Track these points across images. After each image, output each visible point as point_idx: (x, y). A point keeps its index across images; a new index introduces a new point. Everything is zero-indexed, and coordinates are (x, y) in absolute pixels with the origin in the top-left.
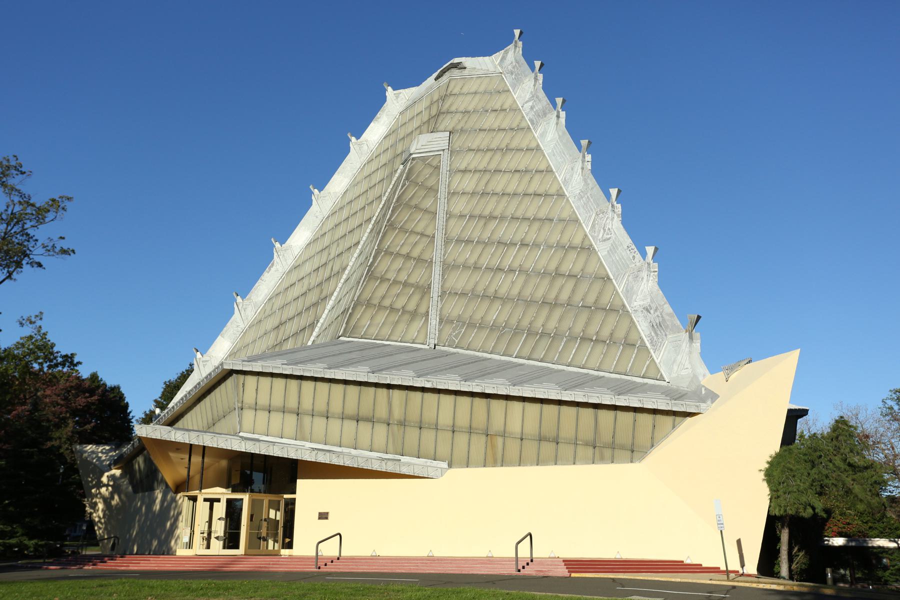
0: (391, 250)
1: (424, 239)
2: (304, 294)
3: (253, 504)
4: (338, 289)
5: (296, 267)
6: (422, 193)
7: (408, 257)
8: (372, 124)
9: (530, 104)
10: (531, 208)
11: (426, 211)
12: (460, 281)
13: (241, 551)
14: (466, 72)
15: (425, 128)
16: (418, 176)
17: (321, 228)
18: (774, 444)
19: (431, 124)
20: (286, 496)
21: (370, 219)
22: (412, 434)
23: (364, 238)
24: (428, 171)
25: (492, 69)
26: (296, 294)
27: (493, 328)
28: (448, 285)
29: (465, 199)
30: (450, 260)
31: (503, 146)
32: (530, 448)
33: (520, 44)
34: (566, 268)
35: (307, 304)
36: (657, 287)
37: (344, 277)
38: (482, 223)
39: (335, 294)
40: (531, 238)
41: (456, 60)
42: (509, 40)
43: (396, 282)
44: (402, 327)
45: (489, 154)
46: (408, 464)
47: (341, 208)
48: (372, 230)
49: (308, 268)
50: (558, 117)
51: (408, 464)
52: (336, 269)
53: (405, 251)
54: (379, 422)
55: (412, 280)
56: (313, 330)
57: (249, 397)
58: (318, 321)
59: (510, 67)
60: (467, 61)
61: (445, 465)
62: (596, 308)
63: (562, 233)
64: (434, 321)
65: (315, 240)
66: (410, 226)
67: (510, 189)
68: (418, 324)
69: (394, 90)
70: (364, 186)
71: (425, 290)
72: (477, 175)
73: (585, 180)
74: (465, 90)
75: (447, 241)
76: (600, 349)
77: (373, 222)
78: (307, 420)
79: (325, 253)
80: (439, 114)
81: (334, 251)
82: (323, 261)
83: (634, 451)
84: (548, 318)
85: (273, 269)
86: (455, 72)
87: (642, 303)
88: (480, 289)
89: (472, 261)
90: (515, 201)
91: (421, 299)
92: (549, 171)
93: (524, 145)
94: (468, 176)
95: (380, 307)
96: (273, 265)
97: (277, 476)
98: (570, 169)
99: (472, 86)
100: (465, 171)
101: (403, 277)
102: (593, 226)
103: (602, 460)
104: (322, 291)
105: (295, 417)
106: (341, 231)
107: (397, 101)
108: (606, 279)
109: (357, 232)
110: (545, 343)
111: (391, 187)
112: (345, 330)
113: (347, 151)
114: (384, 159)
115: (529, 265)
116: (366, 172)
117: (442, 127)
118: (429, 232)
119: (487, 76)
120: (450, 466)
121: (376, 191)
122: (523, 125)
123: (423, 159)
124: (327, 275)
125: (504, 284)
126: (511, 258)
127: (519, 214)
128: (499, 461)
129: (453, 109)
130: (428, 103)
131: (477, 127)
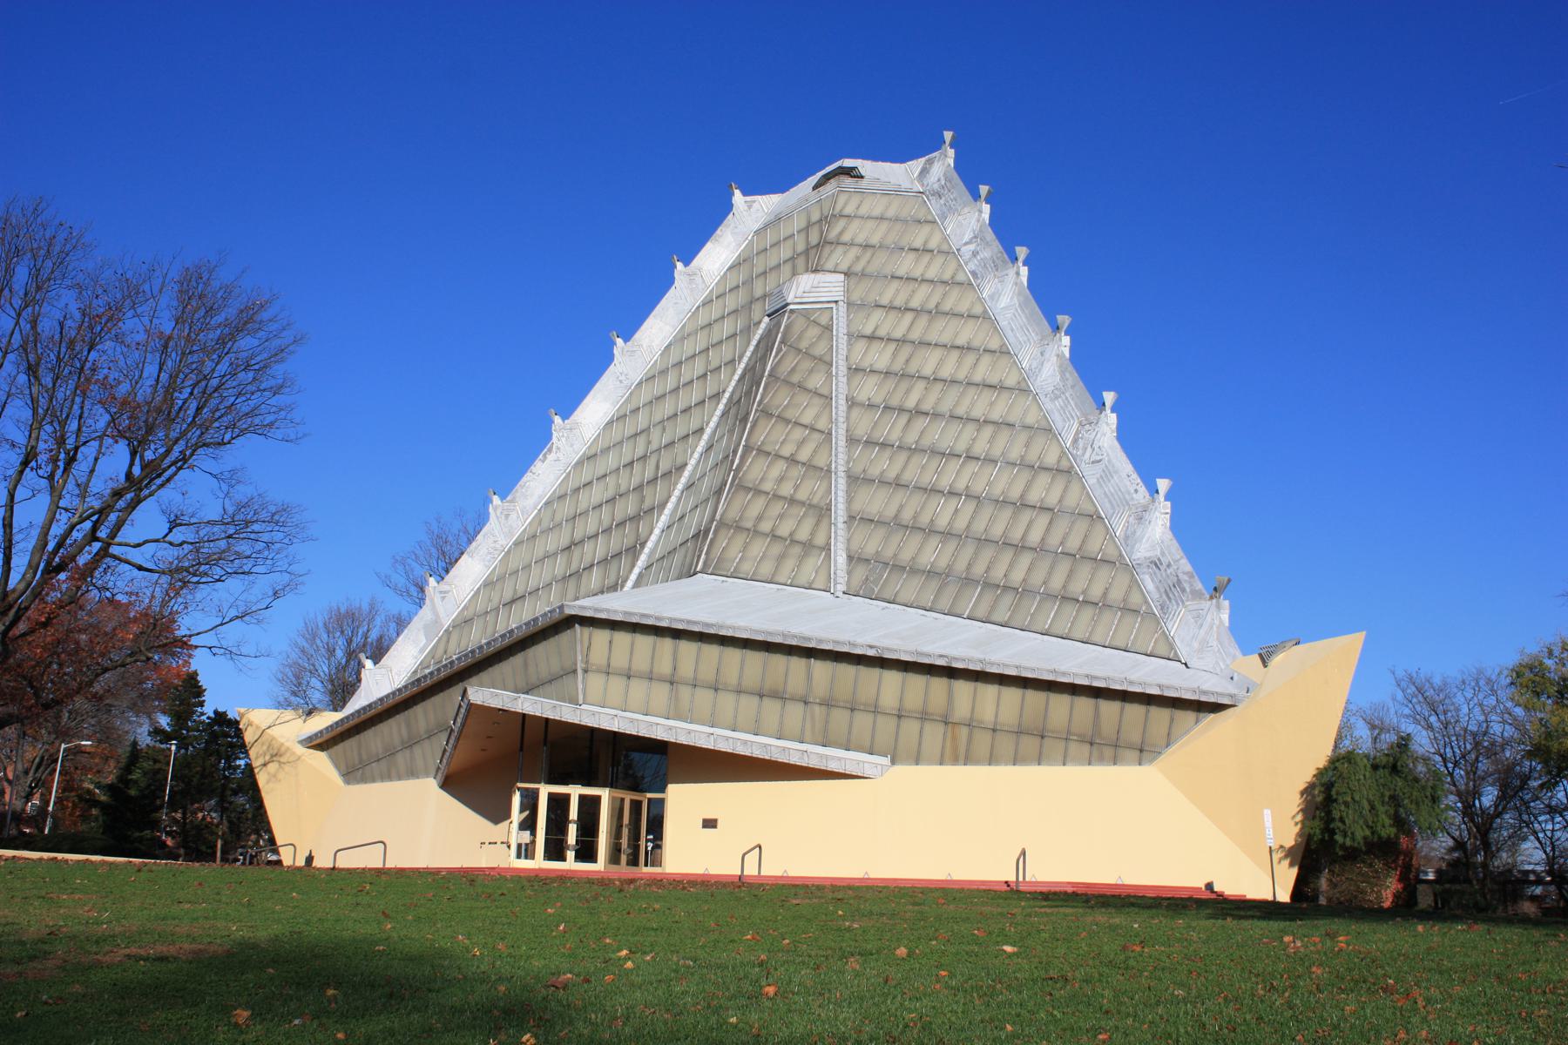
0: (768, 448)
1: (816, 436)
2: (611, 501)
3: (613, 799)
4: (673, 499)
5: (590, 458)
6: (807, 364)
7: (792, 460)
8: (709, 245)
9: (972, 247)
10: (979, 405)
11: (816, 393)
12: (876, 502)
13: (600, 865)
14: (863, 183)
15: (801, 262)
16: (800, 338)
17: (628, 400)
18: (1329, 752)
19: (811, 258)
20: (649, 795)
21: (717, 396)
22: (840, 717)
23: (712, 424)
24: (814, 332)
25: (906, 185)
26: (595, 500)
27: (931, 573)
28: (857, 506)
29: (873, 380)
30: (858, 470)
31: (931, 305)
32: (1006, 744)
33: (951, 152)
34: (1034, 497)
35: (619, 517)
36: (1169, 535)
37: (683, 480)
38: (904, 418)
39: (670, 506)
40: (980, 448)
41: (848, 163)
42: (937, 144)
43: (777, 497)
44: (790, 564)
45: (909, 316)
46: (834, 758)
47: (664, 372)
48: (725, 414)
49: (612, 461)
50: (1018, 274)
51: (834, 758)
52: (664, 466)
53: (787, 451)
54: (792, 699)
55: (802, 495)
56: (635, 559)
57: (599, 655)
58: (643, 545)
59: (936, 186)
60: (865, 166)
61: (886, 761)
62: (1078, 557)
63: (1027, 445)
64: (840, 559)
65: (621, 417)
66: (791, 414)
67: (945, 373)
68: (813, 561)
69: (745, 194)
70: (701, 342)
71: (822, 512)
72: (893, 346)
73: (1062, 373)
74: (863, 211)
75: (852, 441)
76: (1088, 613)
77: (724, 401)
78: (685, 692)
79: (641, 440)
80: (823, 243)
81: (657, 438)
82: (640, 451)
83: (1144, 752)
84: (1011, 565)
85: (551, 457)
86: (848, 181)
87: (1148, 554)
88: (907, 516)
89: (891, 475)
90: (954, 392)
91: (817, 524)
92: (1004, 352)
93: (963, 307)
94: (877, 345)
95: (757, 533)
96: (550, 450)
97: (639, 765)
98: (1045, 358)
99: (875, 206)
100: (872, 338)
101: (786, 490)
102: (1075, 441)
103: (1101, 760)
104: (642, 500)
105: (667, 686)
106: (668, 408)
107: (750, 212)
108: (1094, 518)
109: (696, 412)
110: (1008, 599)
111: (751, 348)
112: (705, 563)
113: (669, 282)
114: (731, 302)
115: (979, 487)
116: (702, 319)
117: (830, 265)
118: (821, 425)
119: (897, 193)
120: (893, 762)
121: (726, 352)
122: (960, 277)
123: (806, 314)
124: (649, 474)
125: (943, 512)
126: (952, 475)
127: (961, 411)
128: (962, 756)
129: (846, 238)
130: (803, 224)
131: (888, 271)
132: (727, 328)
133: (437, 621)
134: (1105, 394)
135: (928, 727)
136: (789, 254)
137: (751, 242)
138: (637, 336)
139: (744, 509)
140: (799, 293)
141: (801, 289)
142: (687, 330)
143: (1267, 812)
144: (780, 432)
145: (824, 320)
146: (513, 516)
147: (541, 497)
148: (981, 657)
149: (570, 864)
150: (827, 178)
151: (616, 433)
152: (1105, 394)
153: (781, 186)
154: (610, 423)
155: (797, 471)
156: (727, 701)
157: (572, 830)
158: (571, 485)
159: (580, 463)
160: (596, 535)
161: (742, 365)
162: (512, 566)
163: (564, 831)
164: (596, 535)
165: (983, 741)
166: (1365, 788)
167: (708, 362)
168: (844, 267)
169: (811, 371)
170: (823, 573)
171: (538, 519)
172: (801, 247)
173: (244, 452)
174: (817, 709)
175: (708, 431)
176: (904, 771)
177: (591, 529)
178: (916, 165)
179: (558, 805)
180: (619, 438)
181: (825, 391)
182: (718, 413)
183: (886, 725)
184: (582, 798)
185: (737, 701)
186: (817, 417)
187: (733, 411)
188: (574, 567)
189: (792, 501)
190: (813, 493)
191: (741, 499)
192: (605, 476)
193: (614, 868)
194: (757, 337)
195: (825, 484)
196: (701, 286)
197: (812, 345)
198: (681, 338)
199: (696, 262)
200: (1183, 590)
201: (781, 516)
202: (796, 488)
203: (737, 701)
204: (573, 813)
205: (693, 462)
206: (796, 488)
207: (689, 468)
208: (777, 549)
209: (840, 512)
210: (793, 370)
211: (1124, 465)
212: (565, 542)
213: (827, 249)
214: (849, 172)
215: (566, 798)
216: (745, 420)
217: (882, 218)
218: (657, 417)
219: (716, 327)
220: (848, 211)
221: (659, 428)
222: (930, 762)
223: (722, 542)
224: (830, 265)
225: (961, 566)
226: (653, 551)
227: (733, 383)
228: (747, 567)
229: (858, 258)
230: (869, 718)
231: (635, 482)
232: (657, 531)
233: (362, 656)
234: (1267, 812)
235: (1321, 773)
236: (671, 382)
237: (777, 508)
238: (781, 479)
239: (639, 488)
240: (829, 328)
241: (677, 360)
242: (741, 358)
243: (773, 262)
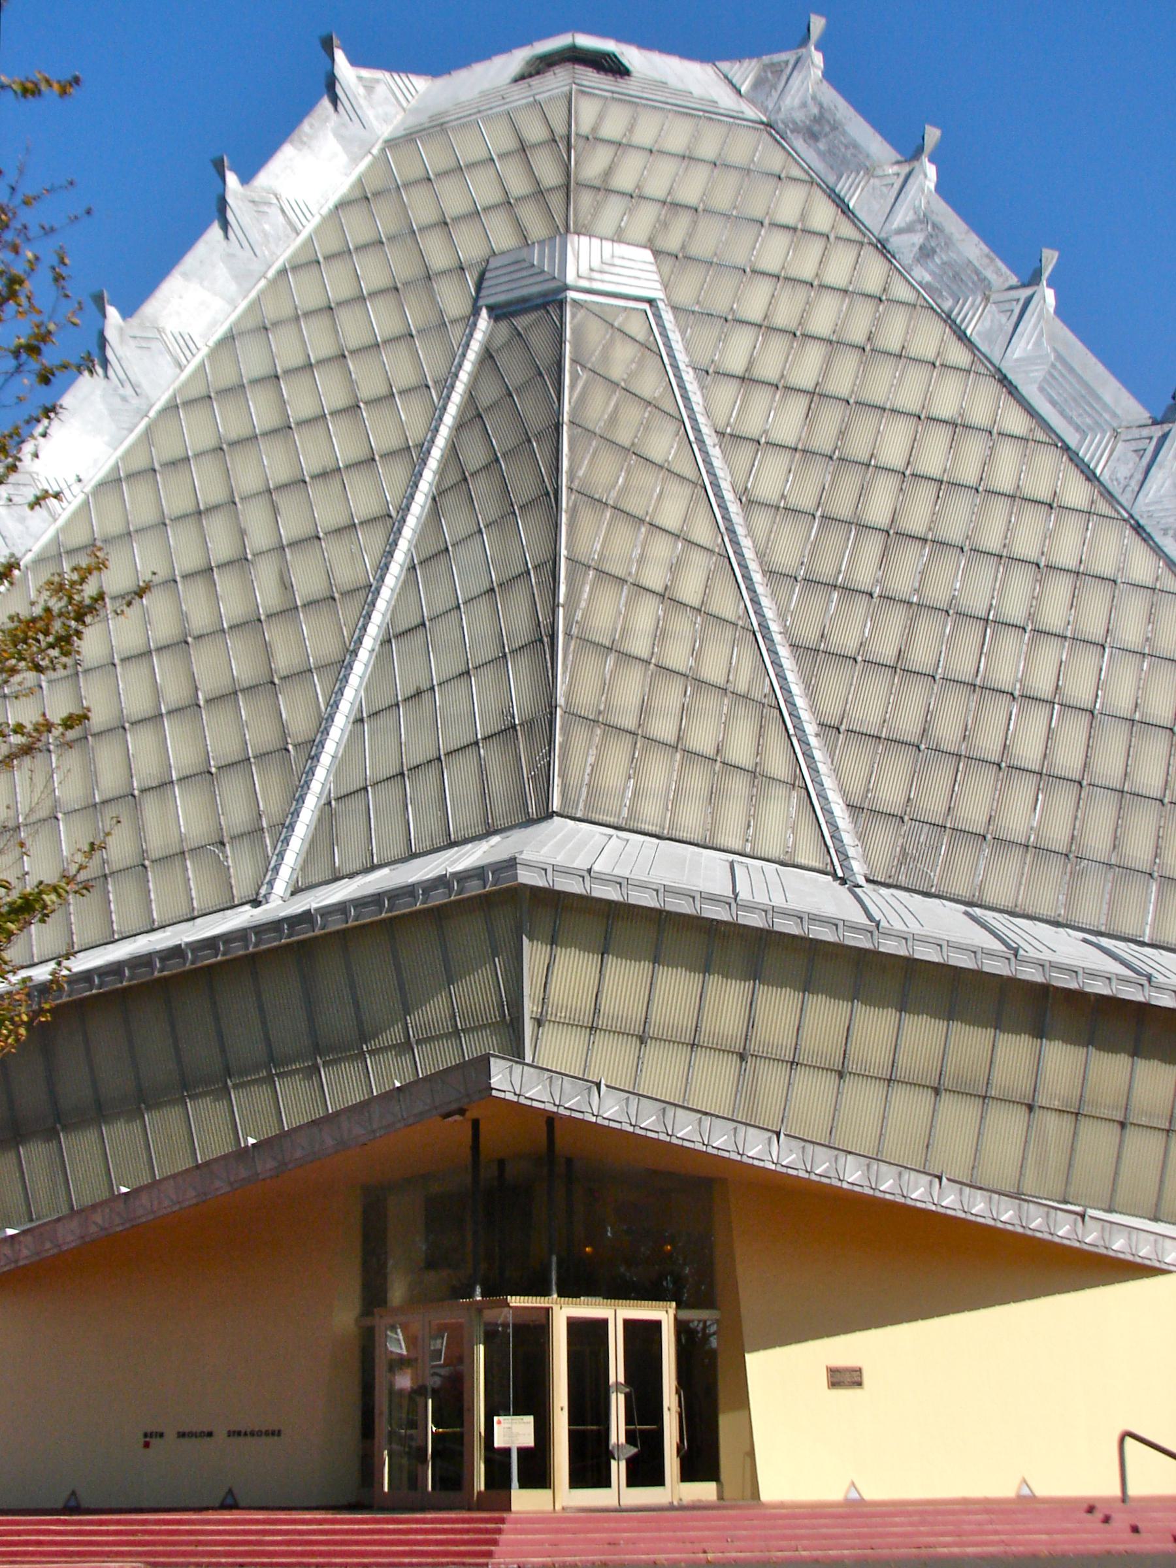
3: (681, 1327)
60: (631, 55)
78: (772, 1078)
86: (590, 77)
143: (386, 1489)
150: (545, 63)
153: (435, 62)
156: (863, 1100)
157: (618, 1405)
178: (745, 72)
184: (631, 1326)
198: (257, 327)
214: (613, 67)
215: (601, 1326)
234: (386, 1489)
236: (260, 412)
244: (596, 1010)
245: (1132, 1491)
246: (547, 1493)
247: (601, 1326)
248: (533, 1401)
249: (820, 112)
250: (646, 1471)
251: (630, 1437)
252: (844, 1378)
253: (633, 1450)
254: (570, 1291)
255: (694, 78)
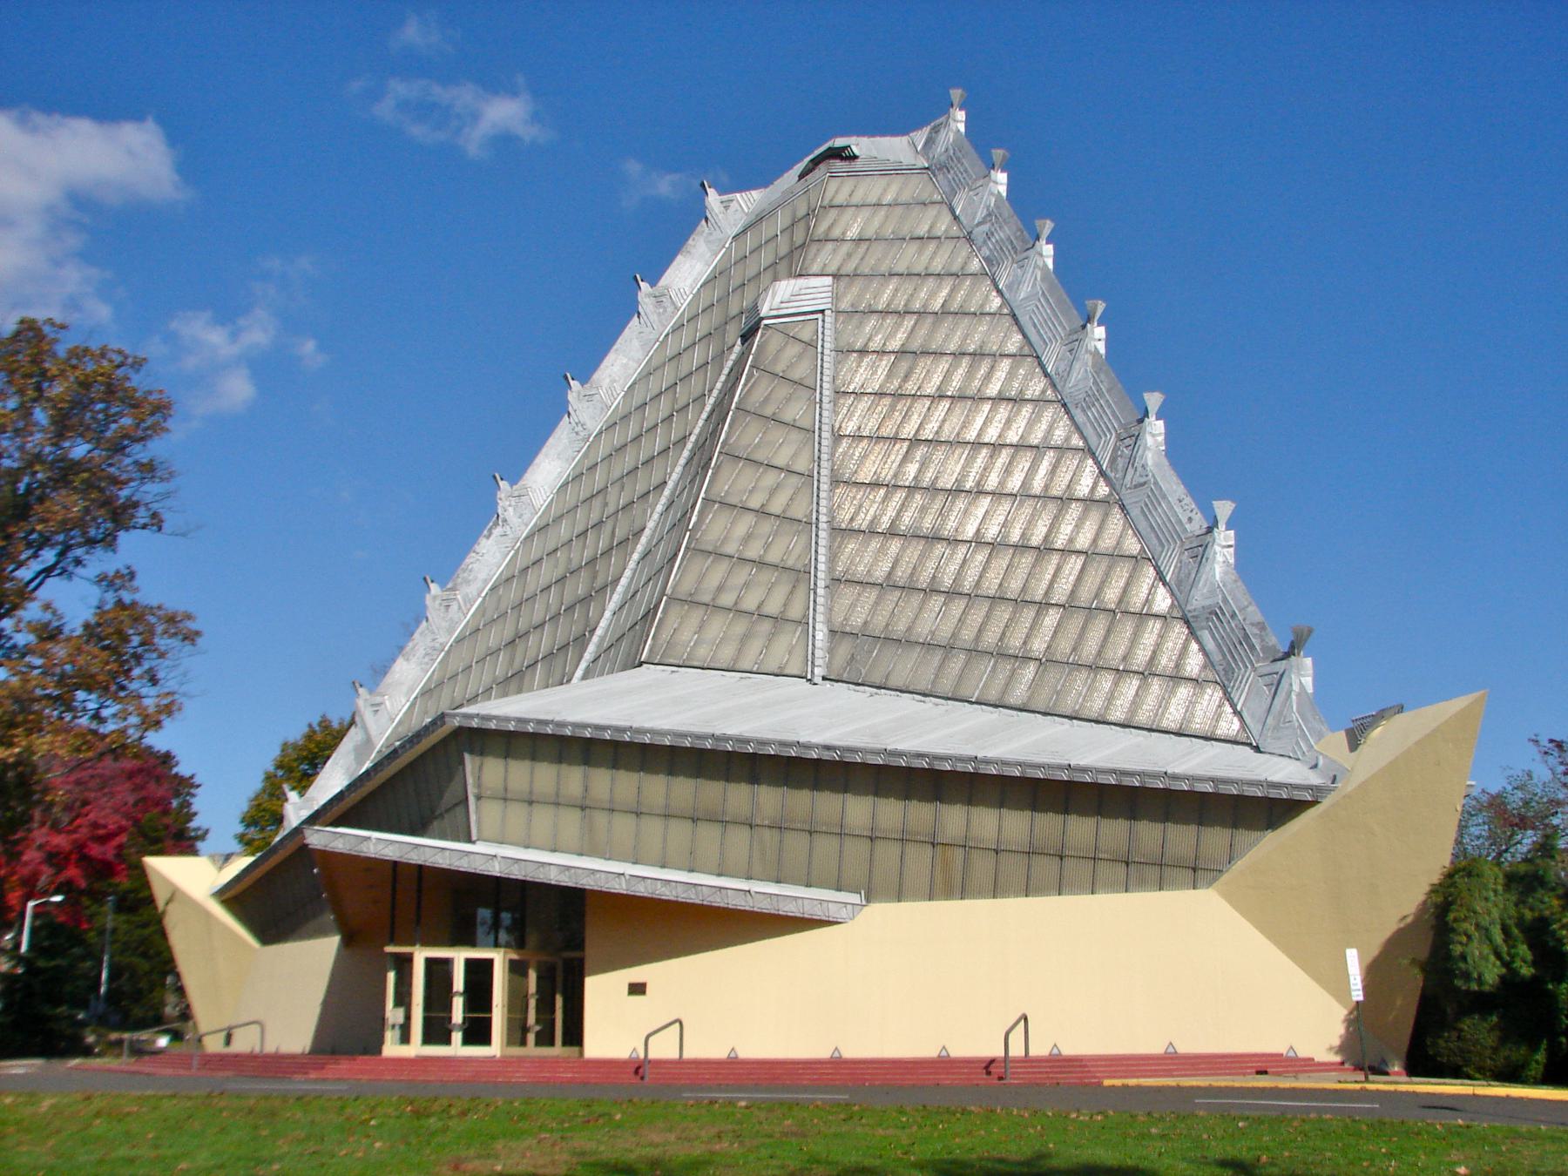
1: (794, 480)
4: (628, 573)
5: (542, 529)
6: (783, 391)
7: (762, 513)
8: (679, 258)
9: (985, 228)
13: (495, 1048)
15: (783, 267)
16: (776, 359)
19: (792, 263)
23: (675, 476)
24: (793, 350)
32: (1013, 867)
35: (568, 598)
37: (640, 548)
39: (624, 581)
41: (839, 142)
47: (626, 417)
49: (564, 531)
51: (763, 893)
55: (774, 556)
58: (593, 631)
59: (943, 158)
60: (860, 145)
61: (854, 898)
65: (577, 477)
68: (788, 638)
70: (668, 375)
71: (801, 575)
77: (689, 446)
78: (601, 819)
79: (597, 503)
80: (810, 241)
81: (616, 499)
82: (594, 517)
83: (1197, 872)
85: (497, 531)
86: (838, 165)
87: (1207, 602)
103: (1142, 885)
111: (723, 378)
112: (651, 650)
114: (703, 326)
119: (898, 171)
120: (868, 900)
121: (695, 384)
130: (788, 222)
132: (697, 357)
133: (368, 742)
134: (1146, 396)
135: (911, 849)
136: (770, 259)
137: (730, 248)
138: (595, 376)
139: (701, 579)
140: (776, 304)
141: (778, 299)
142: (654, 364)
144: (747, 477)
145: (806, 335)
146: (454, 606)
147: (486, 582)
148: (972, 753)
149: (457, 1048)
150: (816, 162)
151: (570, 498)
152: (1146, 396)
153: (763, 181)
154: (565, 484)
155: (767, 527)
156: (653, 827)
157: (458, 1004)
158: (519, 565)
159: (530, 537)
160: (542, 625)
161: (712, 400)
162: (451, 668)
163: (448, 1008)
164: (542, 625)
165: (982, 865)
166: (1491, 907)
167: (675, 400)
168: (832, 269)
169: (788, 399)
170: (799, 652)
171: (482, 610)
172: (784, 250)
173: (132, 546)
174: (767, 833)
175: (670, 484)
176: (883, 913)
177: (537, 618)
178: (920, 137)
179: (438, 972)
180: (573, 503)
181: (806, 424)
182: (682, 461)
183: (856, 850)
184: (430, 962)
185: (666, 827)
186: (795, 455)
187: (695, 462)
188: (516, 666)
189: (761, 564)
190: (787, 552)
191: (699, 565)
192: (556, 550)
193: (517, 1051)
194: (730, 363)
195: (804, 539)
196: (670, 309)
197: (791, 366)
199: (663, 282)
200: (1252, 647)
201: (746, 585)
202: (767, 546)
203: (666, 827)
204: (459, 983)
205: (651, 525)
206: (767, 546)
207: (647, 532)
208: (740, 627)
209: (821, 575)
210: (767, 399)
211: (1173, 488)
212: (508, 633)
213: (814, 248)
215: (447, 963)
216: (706, 466)
217: (879, 205)
218: (616, 474)
219: (685, 357)
220: (840, 200)
221: (617, 487)
222: (916, 896)
223: (673, 621)
224: (815, 268)
225: (967, 635)
226: (602, 639)
227: (701, 423)
228: (703, 653)
229: (849, 255)
230: (834, 842)
231: (587, 554)
232: (608, 614)
233: (286, 787)
235: (1434, 890)
237: (742, 575)
238: (747, 538)
239: (592, 561)
240: (811, 344)
241: (640, 402)
242: (711, 391)
243: (751, 272)
244: (506, 790)
245: (1011, 1054)
246: (576, 1049)
247: (447, 963)
248: (403, 999)
249: (54, 407)
250: (545, 1039)
251: (538, 1021)
252: (637, 989)
253: (538, 1028)
254: (427, 943)
255: (896, 148)
